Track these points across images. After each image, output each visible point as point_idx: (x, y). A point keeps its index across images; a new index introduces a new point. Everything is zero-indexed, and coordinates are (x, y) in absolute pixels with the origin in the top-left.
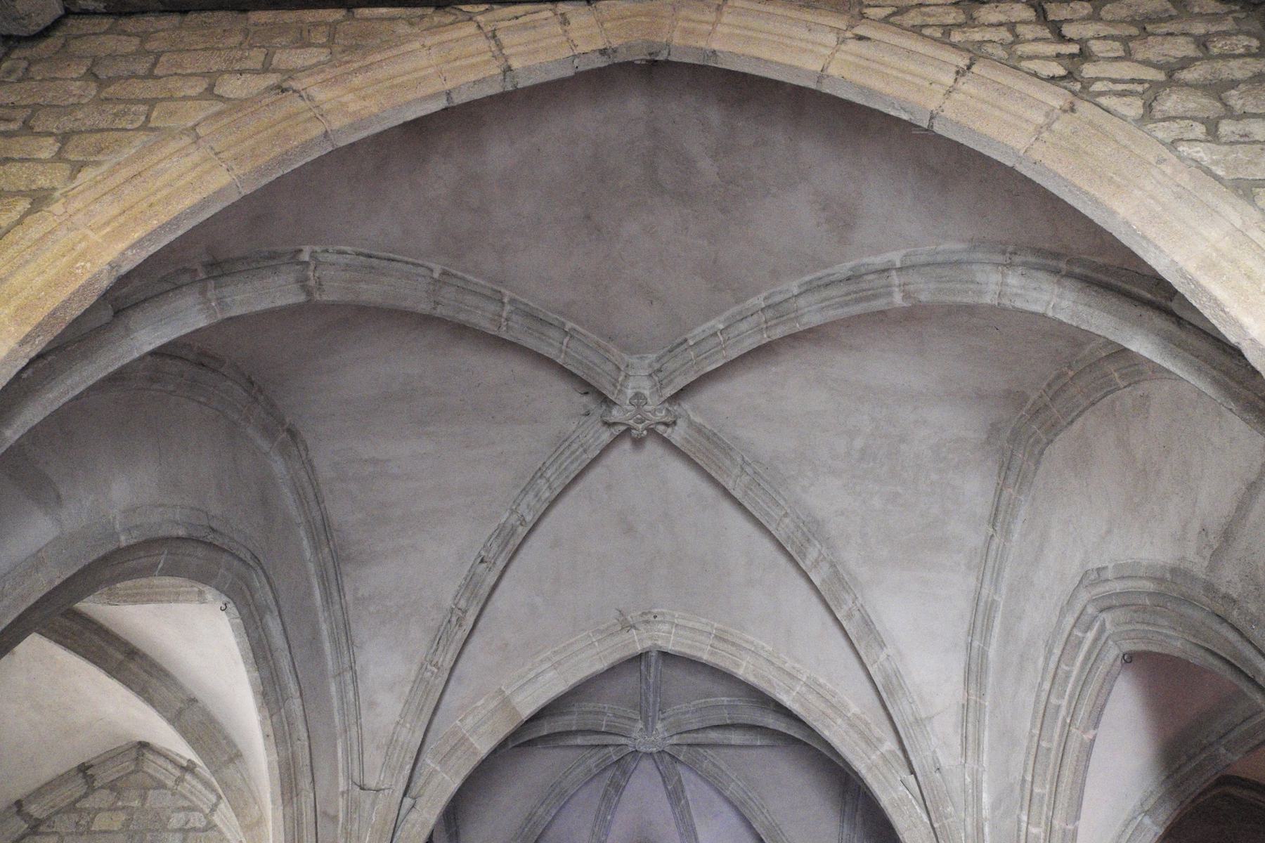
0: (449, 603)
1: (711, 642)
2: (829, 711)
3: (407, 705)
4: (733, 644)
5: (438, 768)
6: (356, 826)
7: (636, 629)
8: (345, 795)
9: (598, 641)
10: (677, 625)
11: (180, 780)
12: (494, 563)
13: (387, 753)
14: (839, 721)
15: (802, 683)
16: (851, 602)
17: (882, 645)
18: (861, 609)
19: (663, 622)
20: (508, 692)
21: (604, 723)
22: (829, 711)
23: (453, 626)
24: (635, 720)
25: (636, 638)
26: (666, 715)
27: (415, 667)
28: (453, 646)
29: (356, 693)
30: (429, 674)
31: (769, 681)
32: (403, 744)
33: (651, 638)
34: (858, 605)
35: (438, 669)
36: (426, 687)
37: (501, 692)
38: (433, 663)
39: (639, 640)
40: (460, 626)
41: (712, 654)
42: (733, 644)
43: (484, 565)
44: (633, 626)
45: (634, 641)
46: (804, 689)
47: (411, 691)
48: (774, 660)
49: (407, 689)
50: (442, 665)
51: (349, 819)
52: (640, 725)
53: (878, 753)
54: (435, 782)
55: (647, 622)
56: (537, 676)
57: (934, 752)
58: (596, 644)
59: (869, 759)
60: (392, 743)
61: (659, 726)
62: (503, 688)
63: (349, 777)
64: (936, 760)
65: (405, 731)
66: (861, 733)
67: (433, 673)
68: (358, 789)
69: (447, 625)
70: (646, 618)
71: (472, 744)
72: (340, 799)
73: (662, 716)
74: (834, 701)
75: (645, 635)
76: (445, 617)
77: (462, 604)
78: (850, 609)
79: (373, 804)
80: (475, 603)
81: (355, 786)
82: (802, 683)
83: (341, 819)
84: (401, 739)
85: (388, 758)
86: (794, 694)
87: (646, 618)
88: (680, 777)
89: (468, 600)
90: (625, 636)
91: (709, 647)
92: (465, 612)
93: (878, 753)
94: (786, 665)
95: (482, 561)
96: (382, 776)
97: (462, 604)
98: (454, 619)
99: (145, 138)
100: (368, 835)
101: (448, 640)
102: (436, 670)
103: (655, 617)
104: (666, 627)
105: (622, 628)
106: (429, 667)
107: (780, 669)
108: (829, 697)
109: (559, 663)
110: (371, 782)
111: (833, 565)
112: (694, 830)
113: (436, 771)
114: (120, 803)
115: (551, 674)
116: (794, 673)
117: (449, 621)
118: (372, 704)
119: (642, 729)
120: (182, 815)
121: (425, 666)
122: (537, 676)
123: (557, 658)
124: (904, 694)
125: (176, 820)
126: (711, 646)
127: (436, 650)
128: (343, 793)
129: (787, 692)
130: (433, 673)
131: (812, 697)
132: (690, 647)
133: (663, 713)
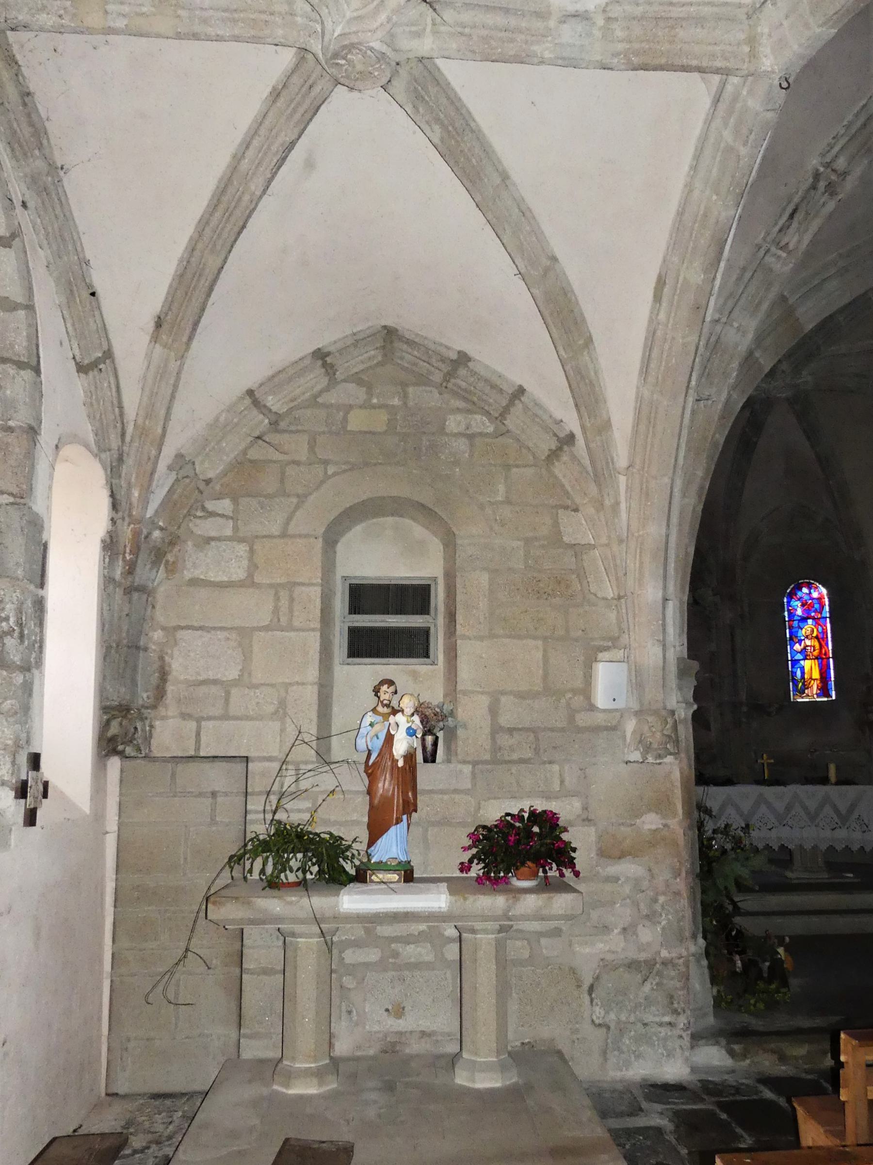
11: (450, 375)
98: (822, 185)
106: (773, 249)
114: (375, 401)
120: (459, 417)
125: (454, 423)
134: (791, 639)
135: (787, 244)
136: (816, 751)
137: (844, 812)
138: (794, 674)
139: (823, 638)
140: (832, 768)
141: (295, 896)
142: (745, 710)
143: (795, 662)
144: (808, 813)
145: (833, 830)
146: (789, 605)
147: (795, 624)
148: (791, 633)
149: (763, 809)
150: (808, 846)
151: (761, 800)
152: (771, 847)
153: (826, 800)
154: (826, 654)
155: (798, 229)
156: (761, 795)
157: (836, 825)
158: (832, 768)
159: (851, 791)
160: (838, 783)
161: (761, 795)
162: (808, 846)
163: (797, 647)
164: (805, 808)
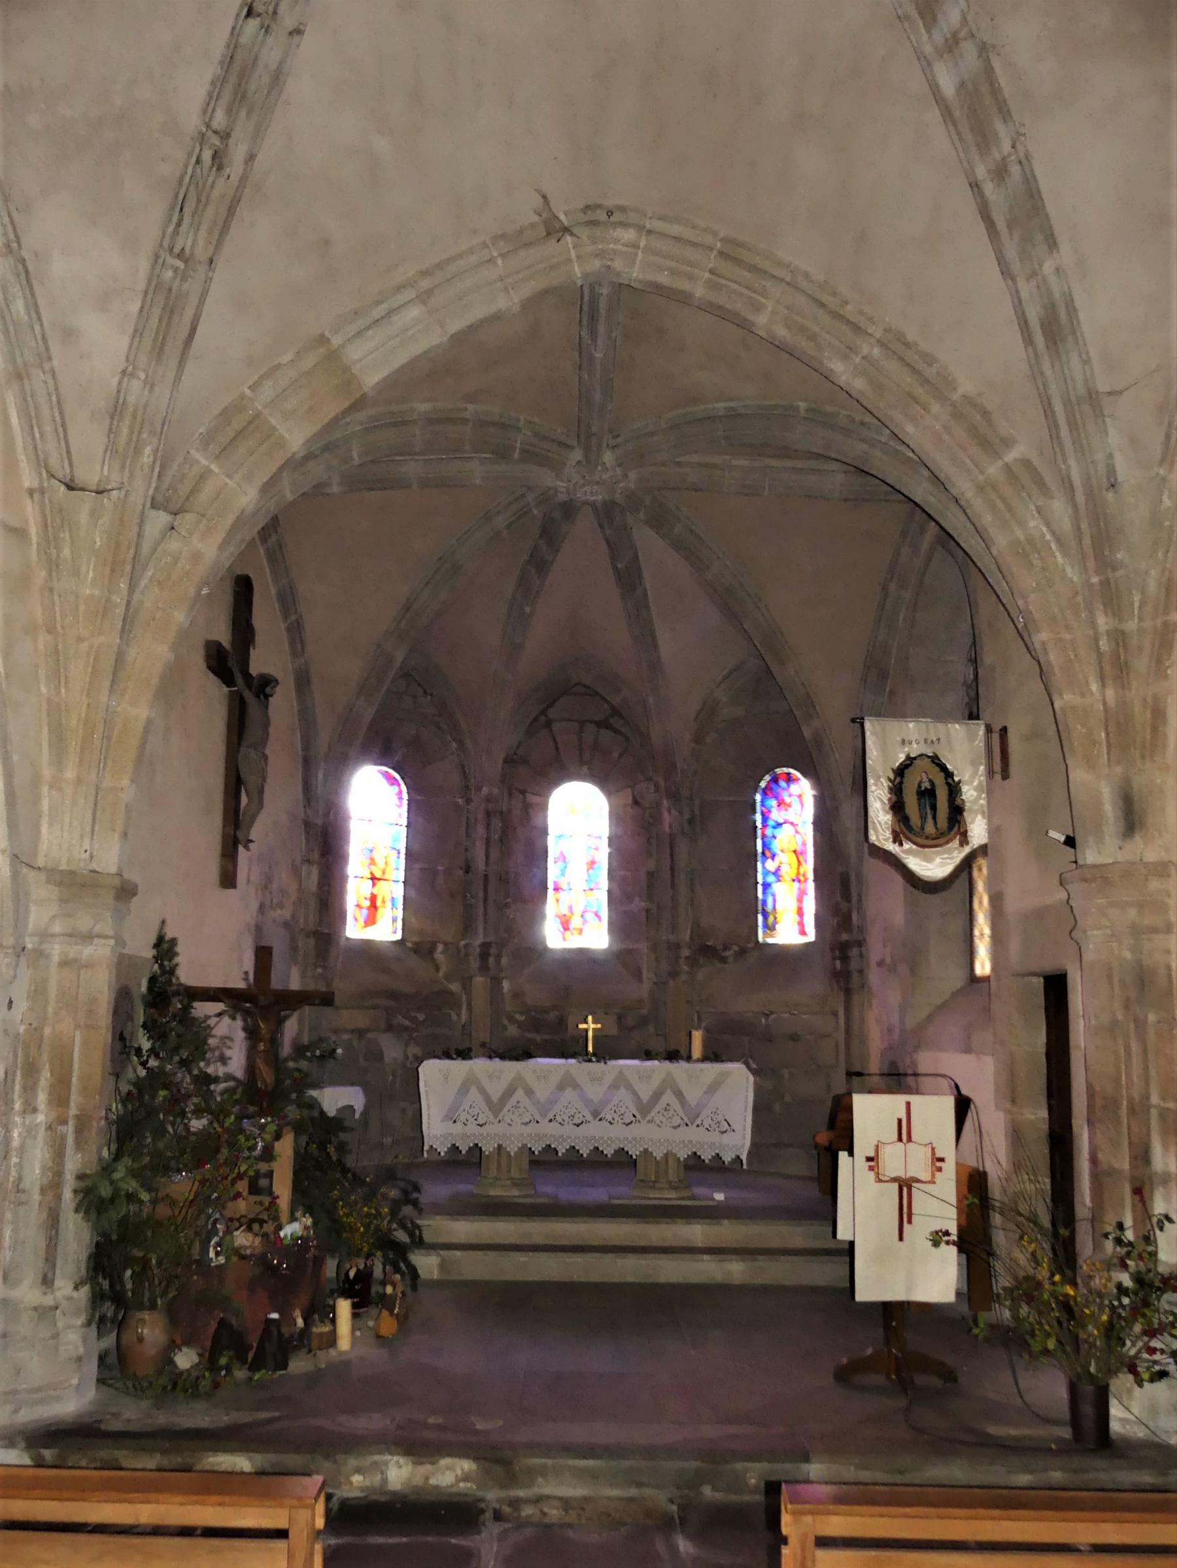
0: (192, 121)
1: (711, 265)
2: (919, 391)
3: (137, 340)
4: (753, 269)
5: (213, 467)
6: (66, 552)
7: (572, 234)
8: (36, 496)
9: (503, 256)
10: (649, 232)
12: (275, 13)
13: (111, 429)
14: (936, 408)
15: (873, 340)
16: (1006, 147)
17: (1052, 243)
18: (1024, 162)
19: (623, 225)
20: (336, 341)
21: (518, 445)
22: (919, 391)
23: (205, 171)
24: (571, 448)
25: (573, 254)
26: (619, 440)
27: (144, 264)
28: (209, 213)
29: (34, 307)
30: (169, 274)
31: (813, 338)
32: (135, 411)
33: (599, 255)
34: (1021, 155)
35: (186, 261)
36: (167, 299)
37: (322, 340)
38: (177, 250)
39: (578, 257)
40: (220, 168)
41: (712, 286)
42: (753, 269)
43: (253, 23)
44: (566, 230)
45: (570, 260)
46: (876, 351)
47: (141, 310)
48: (826, 299)
49: (135, 307)
50: (192, 254)
51: (49, 539)
52: (577, 455)
53: (1000, 463)
54: (208, 490)
55: (594, 223)
56: (390, 313)
57: (1111, 456)
58: (499, 261)
59: (982, 473)
60: (116, 410)
61: (608, 457)
62: (327, 333)
63: (41, 463)
64: (1111, 471)
65: (136, 385)
66: (973, 430)
67: (176, 270)
68: (63, 488)
69: (194, 168)
70: (591, 216)
71: (274, 429)
72: (28, 502)
73: (612, 442)
74: (931, 372)
75: (589, 249)
76: (190, 155)
77: (219, 120)
78: (1004, 159)
79: (95, 514)
80: (243, 114)
81: (54, 481)
82: (873, 340)
83: (33, 531)
84: (132, 399)
85: (112, 435)
86: (858, 360)
87: (591, 216)
88: (636, 554)
89: (229, 111)
90: (552, 246)
91: (707, 275)
92: (225, 136)
93: (1000, 463)
94: (849, 307)
95: (249, 14)
96: (106, 468)
97: (219, 120)
98: (207, 155)
99: (270, 384)
100: (92, 567)
101: (199, 201)
102: (181, 265)
103: (610, 213)
104: (629, 235)
105: (549, 234)
107: (837, 316)
108: (920, 365)
109: (429, 293)
110: (89, 475)
111: (983, 49)
112: (653, 633)
113: (210, 471)
115: (415, 312)
116: (862, 322)
117: (198, 162)
118: (69, 334)
119: (579, 462)
121: (161, 261)
122: (390, 313)
123: (425, 284)
124: (1077, 342)
126: (711, 272)
127: (179, 224)
128: (31, 492)
129: (845, 357)
130: (176, 270)
131: (892, 367)
132: (674, 272)
133: (615, 437)
134: (763, 853)
135: (183, 249)
136: (772, 1013)
137: (495, 1097)
138: (764, 902)
139: (801, 853)
140: (697, 1037)
141: (493, 1197)
142: (687, 954)
143: (766, 886)
144: (488, 1100)
145: (675, 1128)
146: (763, 805)
147: (769, 832)
148: (764, 845)
149: (668, 1097)
150: (658, 1154)
151: (568, 1082)
152: (578, 1151)
153: (669, 1084)
154: (804, 875)
155: (192, 224)
156: (669, 1074)
157: (634, 1119)
158: (697, 1037)
159: (718, 1067)
160: (705, 1058)
161: (669, 1074)
162: (658, 1154)
163: (771, 865)
164: (482, 1091)
